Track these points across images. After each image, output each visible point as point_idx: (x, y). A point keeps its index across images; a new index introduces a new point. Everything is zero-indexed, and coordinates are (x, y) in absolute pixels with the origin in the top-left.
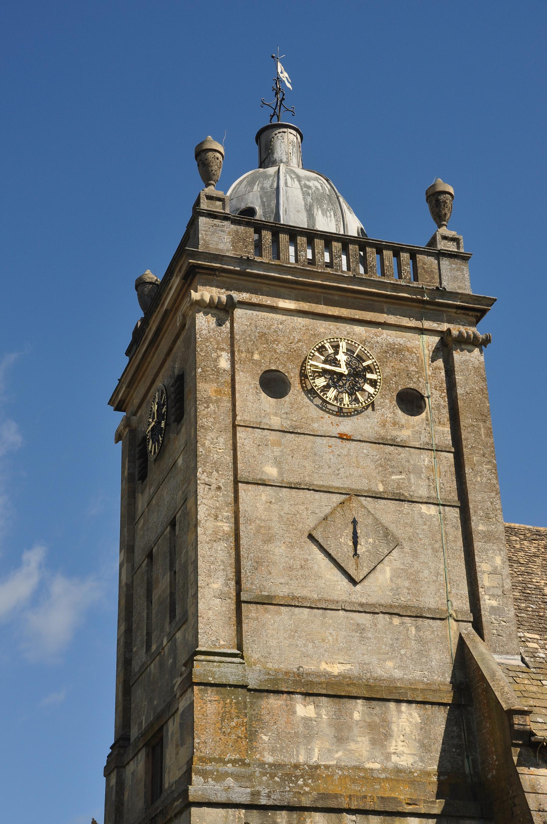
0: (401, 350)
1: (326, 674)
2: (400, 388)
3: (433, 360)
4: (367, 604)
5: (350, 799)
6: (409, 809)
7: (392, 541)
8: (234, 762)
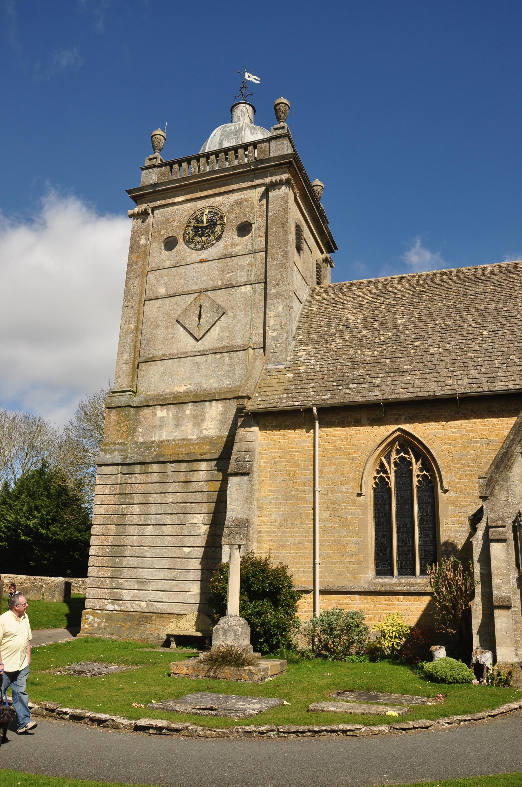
0: (241, 202)
1: (178, 392)
4: (203, 350)
6: (200, 457)
7: (221, 312)
8: (119, 444)
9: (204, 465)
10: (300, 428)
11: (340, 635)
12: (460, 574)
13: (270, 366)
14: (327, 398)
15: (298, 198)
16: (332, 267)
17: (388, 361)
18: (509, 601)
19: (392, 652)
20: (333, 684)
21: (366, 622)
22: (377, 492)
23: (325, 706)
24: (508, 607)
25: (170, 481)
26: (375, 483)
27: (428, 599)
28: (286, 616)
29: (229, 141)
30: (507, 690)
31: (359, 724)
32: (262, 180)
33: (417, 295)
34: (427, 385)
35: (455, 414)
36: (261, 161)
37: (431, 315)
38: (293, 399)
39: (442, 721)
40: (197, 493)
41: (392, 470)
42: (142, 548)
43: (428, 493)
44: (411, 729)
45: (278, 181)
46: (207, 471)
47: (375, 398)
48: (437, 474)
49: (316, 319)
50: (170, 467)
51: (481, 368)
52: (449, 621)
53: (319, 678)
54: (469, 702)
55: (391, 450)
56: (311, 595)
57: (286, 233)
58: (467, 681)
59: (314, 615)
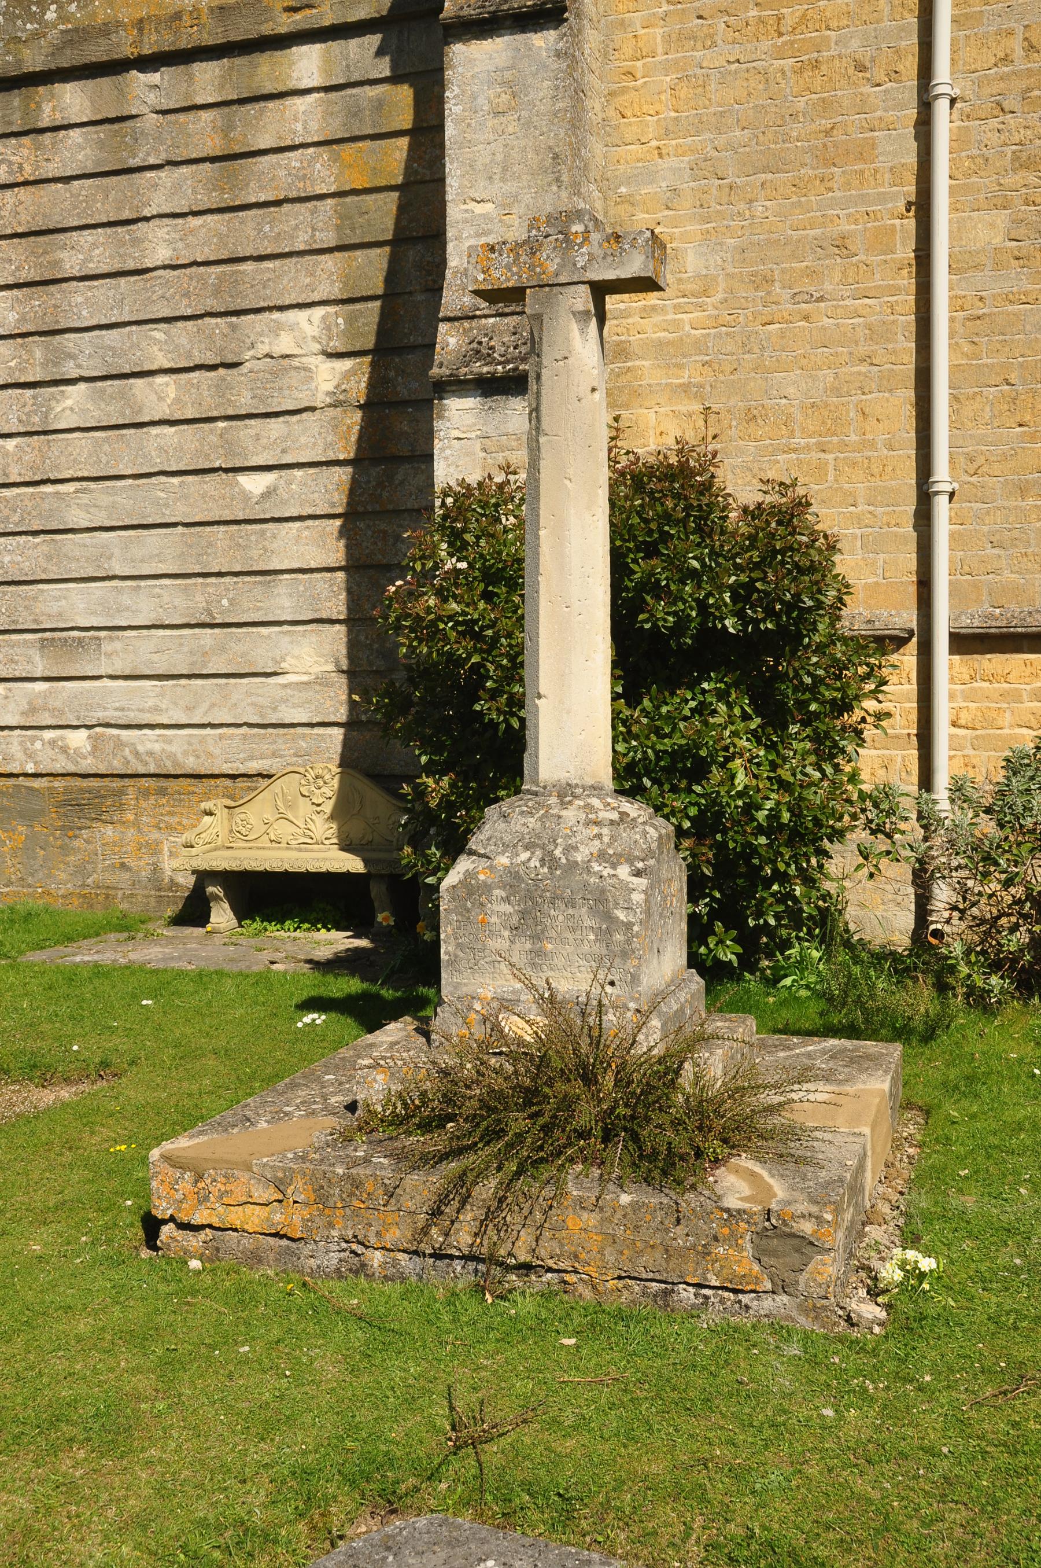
5: (141, 30)
9: (307, 64)
25: (152, 161)
40: (287, 207)
42: (49, 489)
46: (327, 89)
50: (145, 89)
56: (908, 659)
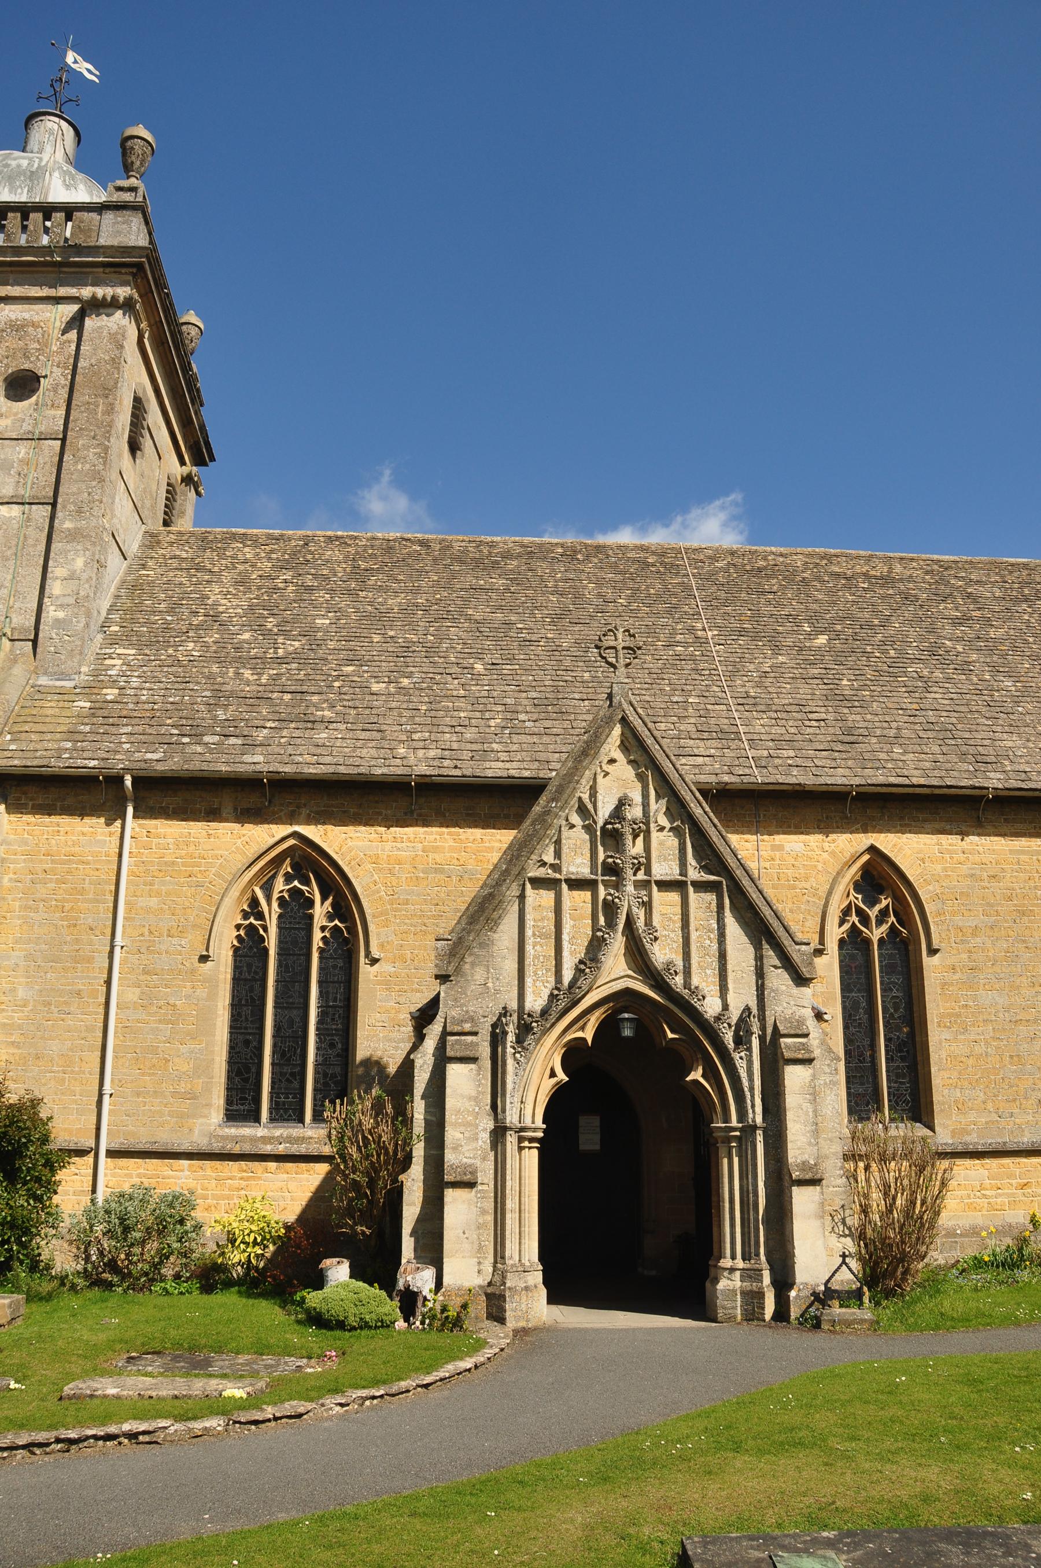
0: (23, 326)
2: (10, 371)
3: (64, 332)
10: (93, 815)
11: (144, 1241)
12: (387, 1121)
13: (43, 681)
14: (158, 760)
15: (146, 341)
16: (198, 494)
17: (287, 697)
18: (474, 1173)
19: (247, 1274)
20: (121, 1341)
21: (198, 1214)
22: (241, 956)
23: (99, 1386)
24: (471, 1185)
26: (239, 937)
27: (323, 1168)
28: (32, 1202)
29: (13, 190)
30: (457, 1337)
31: (166, 1418)
32: (75, 290)
33: (360, 575)
34: (358, 753)
35: (406, 814)
36: (78, 249)
37: (380, 618)
38: (86, 754)
39: (330, 1401)
41: (272, 913)
43: (340, 963)
44: (269, 1420)
45: (109, 299)
47: (252, 768)
48: (360, 927)
49: (152, 596)
51: (464, 730)
52: (360, 1210)
53: (91, 1330)
54: (384, 1363)
55: (275, 873)
57: (110, 410)
58: (385, 1325)
59: (92, 1200)
